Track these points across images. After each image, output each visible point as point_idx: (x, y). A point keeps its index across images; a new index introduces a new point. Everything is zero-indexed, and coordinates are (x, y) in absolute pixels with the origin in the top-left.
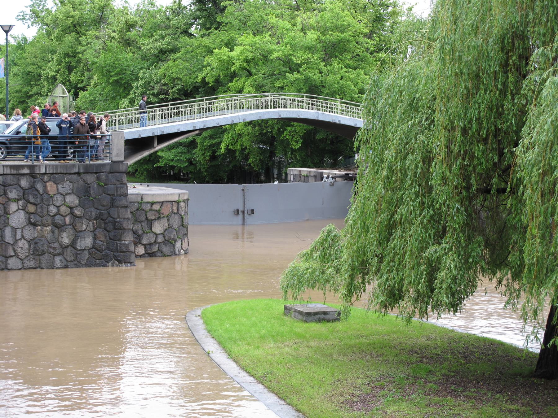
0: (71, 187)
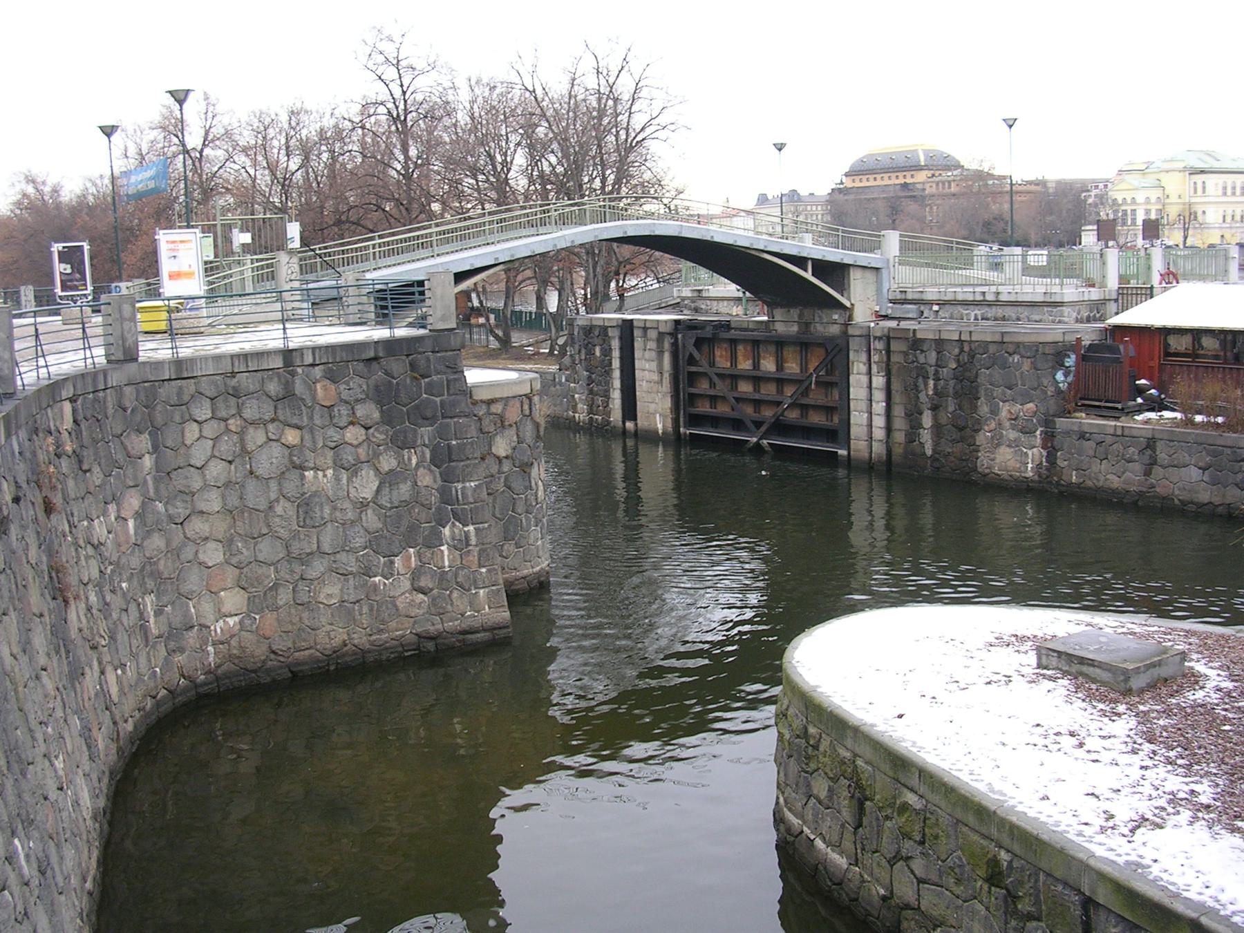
0: (365, 387)
